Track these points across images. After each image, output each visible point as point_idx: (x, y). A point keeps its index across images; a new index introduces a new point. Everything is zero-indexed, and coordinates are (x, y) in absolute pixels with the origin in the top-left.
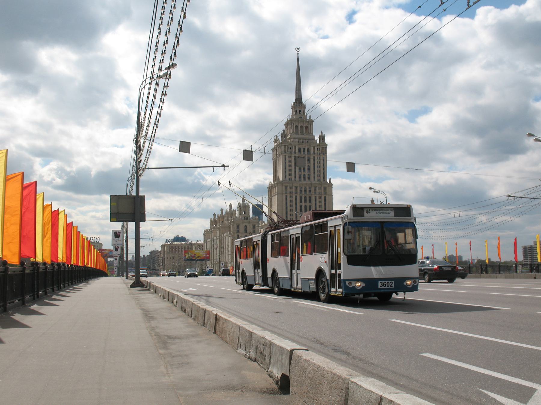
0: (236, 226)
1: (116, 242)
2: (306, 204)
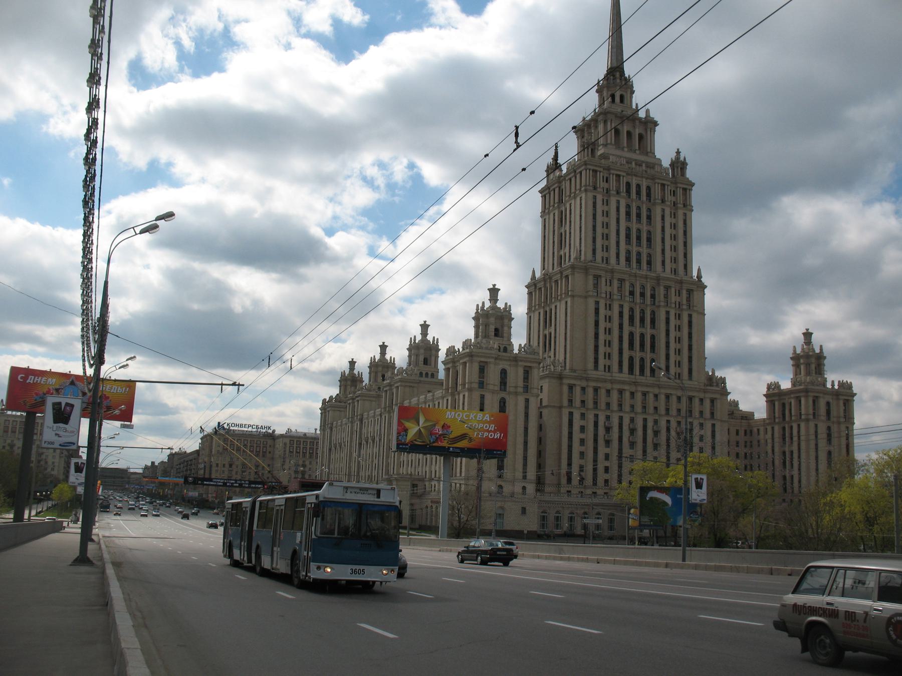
0: (476, 367)
2: (643, 330)
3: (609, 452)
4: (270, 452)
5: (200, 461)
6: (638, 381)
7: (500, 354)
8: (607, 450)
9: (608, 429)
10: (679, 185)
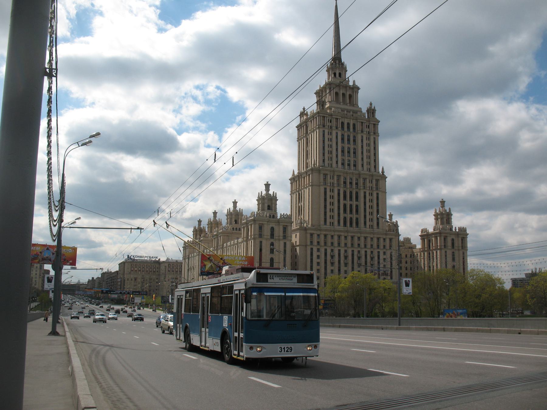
0: (257, 227)
1: (49, 286)
2: (351, 203)
3: (333, 269)
4: (157, 272)
5: (118, 277)
6: (349, 230)
7: (271, 219)
8: (332, 268)
9: (332, 257)
10: (371, 122)
